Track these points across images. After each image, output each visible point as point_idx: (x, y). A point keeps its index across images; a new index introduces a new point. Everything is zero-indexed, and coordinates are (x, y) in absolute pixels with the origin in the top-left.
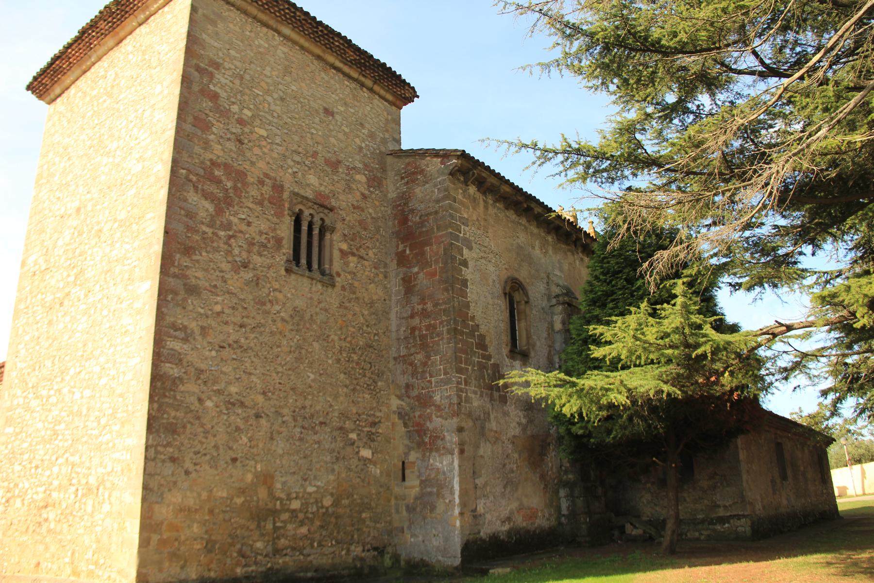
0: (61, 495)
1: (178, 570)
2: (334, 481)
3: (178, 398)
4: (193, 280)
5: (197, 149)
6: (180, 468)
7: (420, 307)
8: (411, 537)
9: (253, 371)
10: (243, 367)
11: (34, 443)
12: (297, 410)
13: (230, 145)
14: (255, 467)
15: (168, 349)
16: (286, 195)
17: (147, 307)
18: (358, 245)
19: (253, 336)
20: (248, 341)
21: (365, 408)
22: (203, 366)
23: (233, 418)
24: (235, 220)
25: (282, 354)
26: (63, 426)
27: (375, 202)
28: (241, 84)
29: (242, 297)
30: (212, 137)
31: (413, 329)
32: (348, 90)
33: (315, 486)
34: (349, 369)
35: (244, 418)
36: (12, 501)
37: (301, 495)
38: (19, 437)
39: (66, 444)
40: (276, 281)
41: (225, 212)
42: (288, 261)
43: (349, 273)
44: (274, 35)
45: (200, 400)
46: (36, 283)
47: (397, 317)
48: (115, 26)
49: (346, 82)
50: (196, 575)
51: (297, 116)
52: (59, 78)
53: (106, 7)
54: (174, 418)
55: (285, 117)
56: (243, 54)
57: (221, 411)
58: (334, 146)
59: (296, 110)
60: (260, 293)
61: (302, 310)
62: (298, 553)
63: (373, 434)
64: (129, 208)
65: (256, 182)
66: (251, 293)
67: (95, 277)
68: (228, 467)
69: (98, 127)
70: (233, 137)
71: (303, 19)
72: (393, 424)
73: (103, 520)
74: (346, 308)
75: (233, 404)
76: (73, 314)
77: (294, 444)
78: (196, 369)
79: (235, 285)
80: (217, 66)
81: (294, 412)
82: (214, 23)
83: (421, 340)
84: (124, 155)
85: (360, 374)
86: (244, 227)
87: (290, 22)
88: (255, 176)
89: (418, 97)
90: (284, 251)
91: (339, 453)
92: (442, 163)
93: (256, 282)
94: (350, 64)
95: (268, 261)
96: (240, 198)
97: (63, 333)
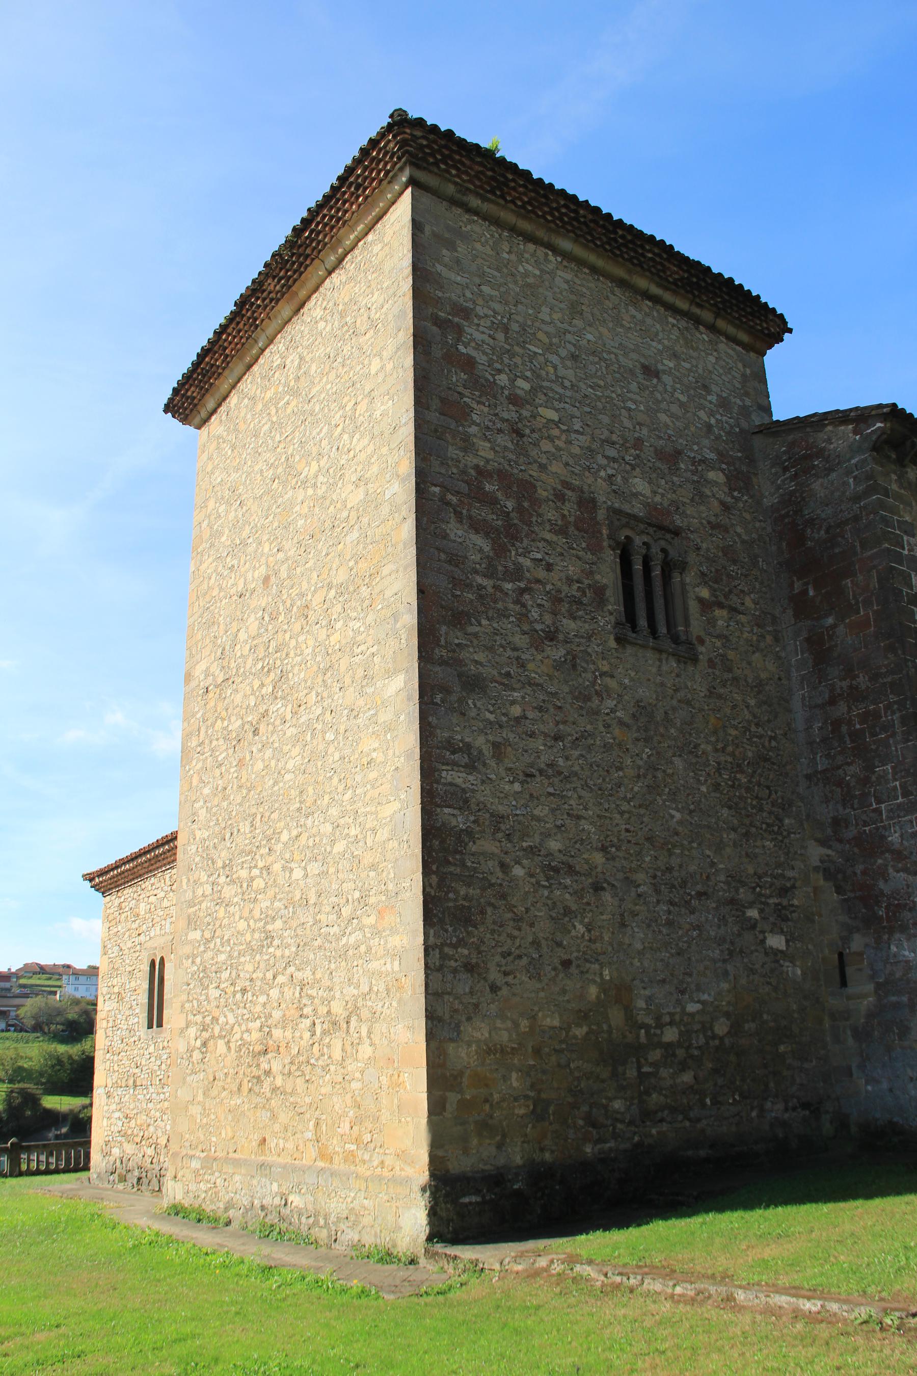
0: (288, 1034)
1: (493, 1150)
2: (729, 991)
3: (469, 864)
4: (472, 667)
5: (453, 452)
6: (482, 981)
7: (845, 684)
8: (867, 1083)
9: (583, 813)
10: (566, 806)
11: (236, 954)
12: (659, 874)
13: (503, 440)
14: (601, 974)
15: (445, 784)
16: (601, 514)
17: (402, 718)
18: (727, 589)
19: (576, 753)
20: (570, 763)
21: (767, 864)
22: (502, 809)
23: (559, 893)
24: (527, 563)
25: (626, 781)
26: (279, 924)
27: (744, 514)
28: (507, 338)
29: (552, 689)
30: (473, 430)
31: (837, 724)
32: (676, 332)
33: (699, 1002)
34: (736, 800)
35: (576, 893)
36: (211, 1042)
37: (677, 1018)
38: (212, 946)
39: (287, 953)
40: (603, 659)
41: (510, 551)
42: (618, 624)
43: (718, 637)
44: (546, 255)
45: (503, 866)
46: (212, 704)
47: (804, 705)
48: (290, 283)
49: (671, 320)
50: (521, 1158)
51: (602, 383)
52: (212, 384)
53: (273, 256)
54: (466, 898)
55: (584, 387)
56: (502, 289)
57: (538, 883)
58: (667, 426)
59: (599, 373)
60: (580, 680)
61: (650, 704)
62: (680, 1117)
63: (784, 908)
64: (351, 563)
65: (551, 497)
66: (566, 682)
67: (306, 681)
68: (557, 975)
69: (281, 446)
70: (505, 426)
71: (591, 221)
72: (816, 889)
73: (362, 1073)
74: (720, 697)
75: (556, 870)
76: (276, 745)
77: (660, 932)
78: (492, 815)
79: (539, 671)
80: (466, 313)
81: (655, 877)
82: (452, 246)
83: (852, 741)
84: (331, 481)
85: (753, 807)
86: (541, 574)
87: (570, 228)
88: (549, 488)
89: (790, 331)
90: (610, 607)
91: (732, 943)
92: (855, 432)
93: (571, 664)
94: (674, 287)
95: (587, 626)
96: (529, 526)
97: (263, 776)
